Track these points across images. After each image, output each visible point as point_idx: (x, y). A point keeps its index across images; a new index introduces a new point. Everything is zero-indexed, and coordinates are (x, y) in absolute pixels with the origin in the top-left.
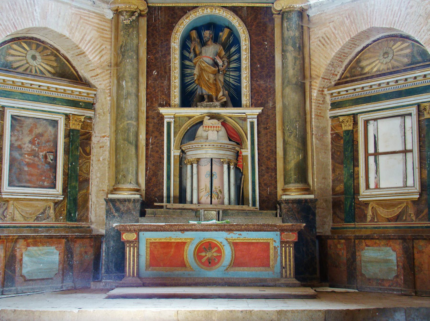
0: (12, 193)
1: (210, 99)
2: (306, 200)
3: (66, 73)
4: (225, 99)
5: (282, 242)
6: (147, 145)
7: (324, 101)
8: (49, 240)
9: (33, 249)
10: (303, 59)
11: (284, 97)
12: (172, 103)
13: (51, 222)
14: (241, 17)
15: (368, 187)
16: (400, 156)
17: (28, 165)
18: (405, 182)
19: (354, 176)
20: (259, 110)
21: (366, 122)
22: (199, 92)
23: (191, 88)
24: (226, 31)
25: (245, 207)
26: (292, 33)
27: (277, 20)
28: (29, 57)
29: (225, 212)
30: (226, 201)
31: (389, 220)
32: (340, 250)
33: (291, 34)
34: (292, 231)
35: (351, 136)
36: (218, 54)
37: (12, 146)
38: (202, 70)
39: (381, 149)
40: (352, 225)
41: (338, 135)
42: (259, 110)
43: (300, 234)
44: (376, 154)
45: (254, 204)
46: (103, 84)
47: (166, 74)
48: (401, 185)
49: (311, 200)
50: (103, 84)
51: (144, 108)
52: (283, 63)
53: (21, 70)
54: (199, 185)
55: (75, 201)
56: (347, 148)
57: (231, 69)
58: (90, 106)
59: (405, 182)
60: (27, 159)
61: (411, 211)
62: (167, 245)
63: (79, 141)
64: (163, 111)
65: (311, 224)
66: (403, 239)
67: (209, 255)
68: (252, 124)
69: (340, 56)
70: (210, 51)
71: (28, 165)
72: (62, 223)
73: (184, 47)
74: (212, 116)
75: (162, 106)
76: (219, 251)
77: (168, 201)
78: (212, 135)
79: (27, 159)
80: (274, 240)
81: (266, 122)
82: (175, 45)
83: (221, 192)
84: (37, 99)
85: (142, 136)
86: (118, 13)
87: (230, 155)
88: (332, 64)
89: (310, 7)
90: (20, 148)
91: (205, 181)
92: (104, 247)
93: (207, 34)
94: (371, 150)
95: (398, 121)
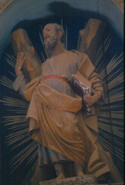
4: (106, 169)
22: (41, 160)
24: (93, 25)
36: (79, 69)
57: (112, 107)
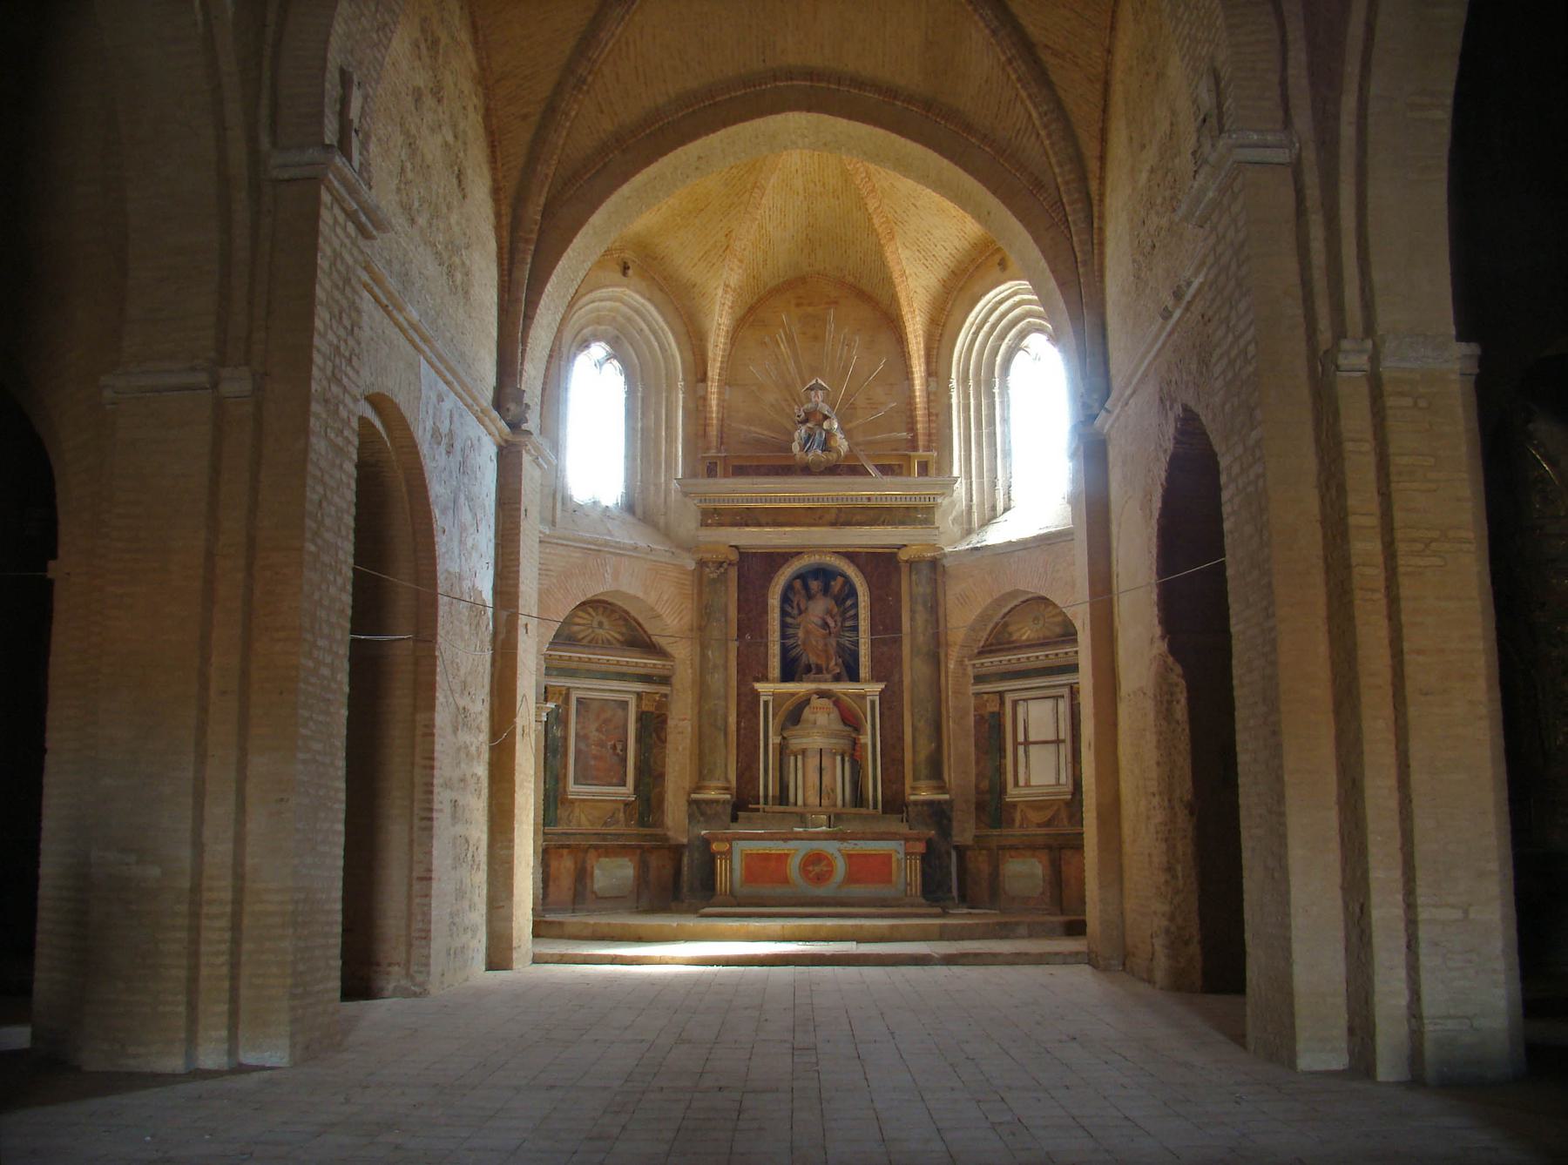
0: (578, 793)
1: (819, 670)
2: (939, 802)
3: (640, 641)
5: (906, 854)
6: (738, 730)
7: (965, 674)
8: (623, 850)
9: (604, 860)
10: (937, 621)
11: (913, 670)
12: (770, 676)
13: (620, 828)
14: (858, 566)
15: (1016, 784)
16: (1052, 748)
17: (595, 757)
18: (1058, 779)
19: (1000, 770)
20: (882, 686)
21: (1015, 703)
22: (804, 660)
23: (793, 653)
24: (840, 580)
25: (863, 811)
26: (922, 589)
27: (905, 569)
28: (595, 624)
29: (838, 816)
30: (839, 802)
31: (1039, 825)
32: (980, 863)
33: (921, 590)
34: (918, 839)
35: (998, 717)
36: (829, 612)
37: (577, 735)
38: (807, 632)
39: (1032, 738)
40: (995, 832)
41: (982, 717)
42: (882, 686)
43: (929, 843)
44: (1027, 743)
45: (875, 806)
46: (682, 653)
47: (763, 633)
48: (1053, 782)
49: (946, 802)
50: (682, 653)
51: (734, 683)
52: (911, 623)
53: (585, 642)
54: (805, 785)
55: (648, 804)
56: (992, 734)
58: (665, 680)
59: (1058, 779)
60: (594, 750)
61: (1064, 815)
62: (766, 857)
63: (653, 725)
64: (759, 686)
65: (945, 830)
66: (1050, 848)
67: (817, 869)
68: (873, 703)
69: (984, 618)
70: (819, 608)
71: (595, 757)
72: (634, 829)
73: (785, 599)
74: (822, 694)
75: (758, 680)
76: (830, 864)
77: (766, 803)
78: (822, 719)
79: (594, 750)
80: (897, 851)
81: (890, 701)
82: (774, 601)
83: (833, 790)
84: (605, 676)
85: (732, 719)
86: (702, 564)
87: (843, 744)
88: (972, 629)
89: (945, 555)
90: (586, 737)
91: (813, 777)
92: (685, 860)
93: (815, 585)
94: (1021, 738)
95: (1049, 704)
